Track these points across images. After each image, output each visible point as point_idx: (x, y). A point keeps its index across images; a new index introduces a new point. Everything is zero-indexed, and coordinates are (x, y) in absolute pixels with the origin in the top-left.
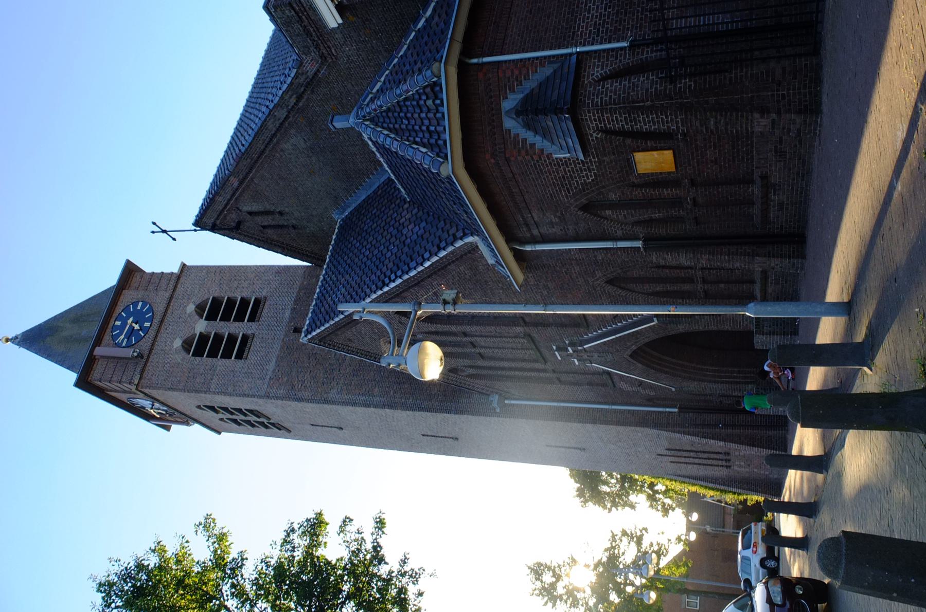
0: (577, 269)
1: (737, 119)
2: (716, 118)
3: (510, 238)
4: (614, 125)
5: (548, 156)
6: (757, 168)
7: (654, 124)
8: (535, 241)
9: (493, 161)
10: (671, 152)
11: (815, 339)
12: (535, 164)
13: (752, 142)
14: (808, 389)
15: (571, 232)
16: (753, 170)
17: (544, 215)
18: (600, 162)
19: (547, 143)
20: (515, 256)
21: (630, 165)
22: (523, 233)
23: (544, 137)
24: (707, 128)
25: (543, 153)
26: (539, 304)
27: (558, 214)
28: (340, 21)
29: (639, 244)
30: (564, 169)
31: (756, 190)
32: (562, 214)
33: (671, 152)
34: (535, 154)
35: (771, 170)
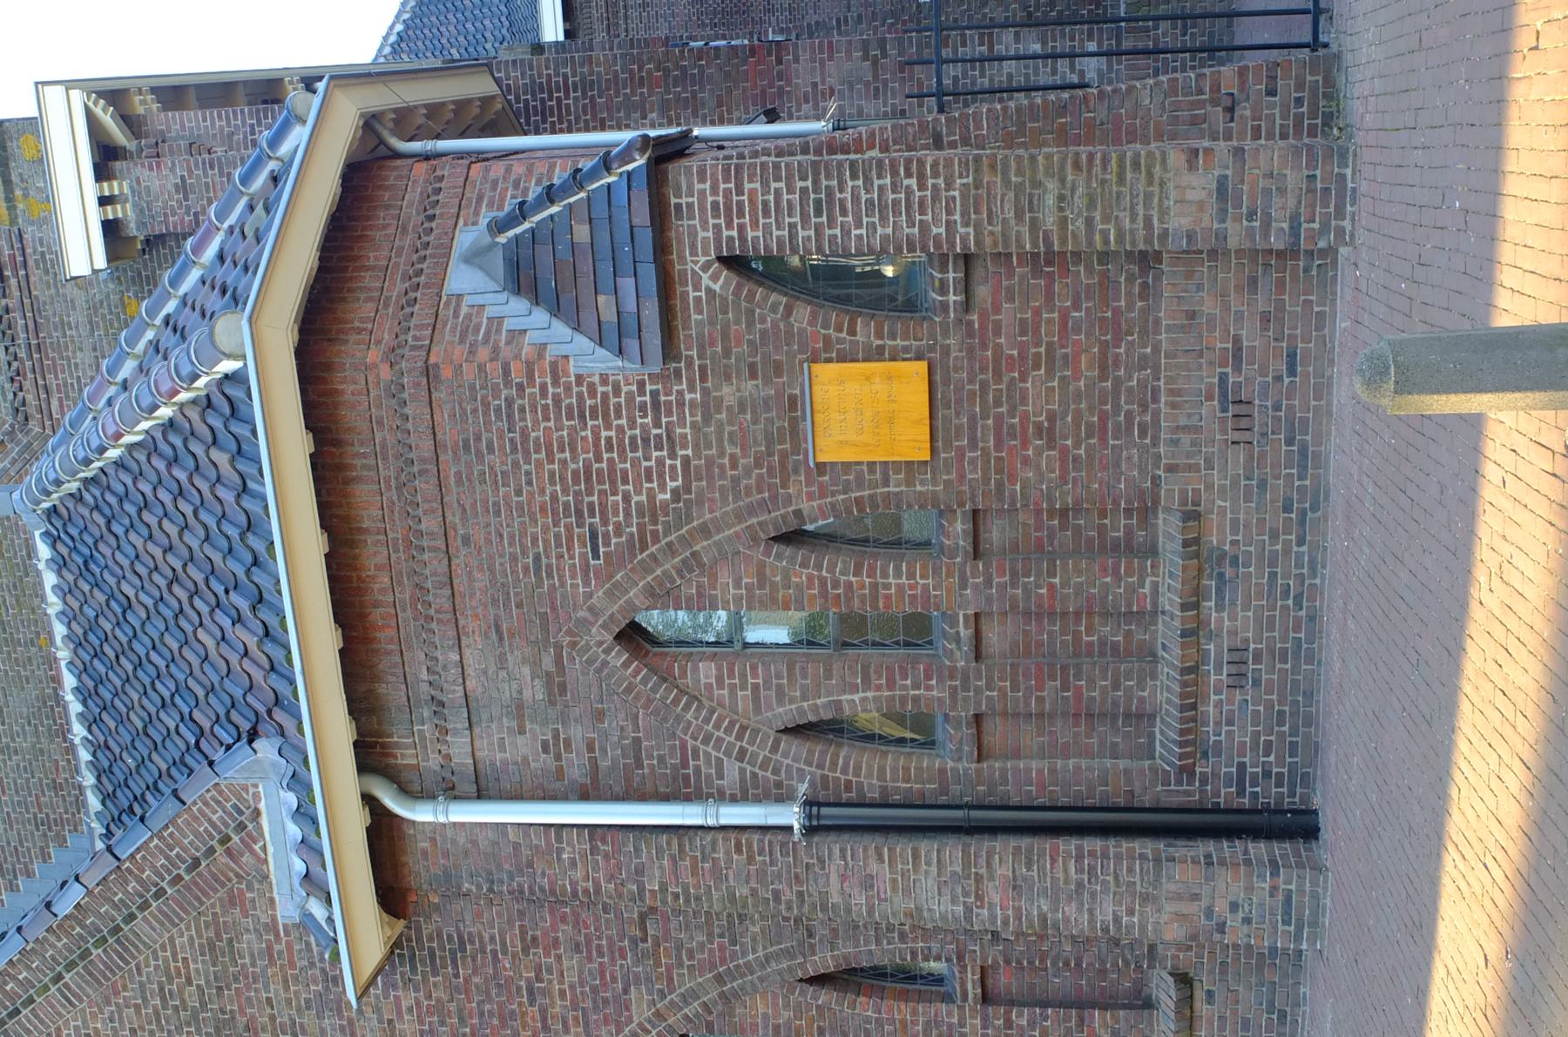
0: (571, 963)
1: (1121, 180)
2: (1062, 180)
3: (371, 755)
4: (741, 228)
5: (554, 365)
6: (1171, 469)
7: (884, 219)
8: (451, 792)
9: (385, 372)
10: (922, 367)
11: (1479, 273)
12: (509, 402)
13: (1156, 349)
14: (1503, 321)
15: (576, 767)
16: (1156, 481)
17: (502, 661)
18: (708, 407)
19: (561, 329)
20: (371, 832)
21: (794, 412)
22: (413, 746)
23: (556, 310)
24: (1034, 225)
25: (541, 356)
26: (396, 50)
27: (548, 663)
28: (101, 262)
29: (790, 816)
30: (597, 438)
31: (1165, 583)
32: (558, 660)
33: (922, 367)
34: (517, 357)
35: (1209, 487)
